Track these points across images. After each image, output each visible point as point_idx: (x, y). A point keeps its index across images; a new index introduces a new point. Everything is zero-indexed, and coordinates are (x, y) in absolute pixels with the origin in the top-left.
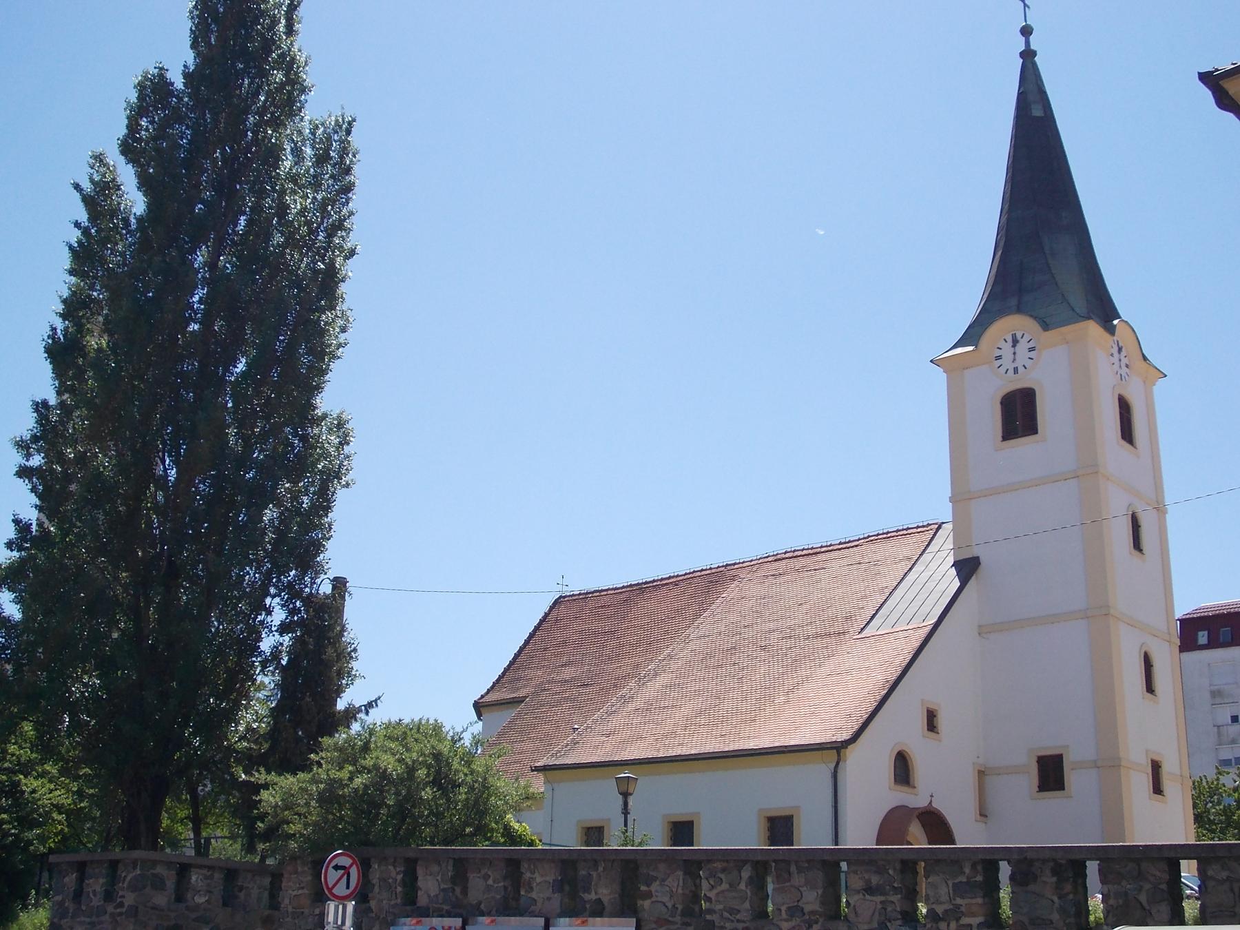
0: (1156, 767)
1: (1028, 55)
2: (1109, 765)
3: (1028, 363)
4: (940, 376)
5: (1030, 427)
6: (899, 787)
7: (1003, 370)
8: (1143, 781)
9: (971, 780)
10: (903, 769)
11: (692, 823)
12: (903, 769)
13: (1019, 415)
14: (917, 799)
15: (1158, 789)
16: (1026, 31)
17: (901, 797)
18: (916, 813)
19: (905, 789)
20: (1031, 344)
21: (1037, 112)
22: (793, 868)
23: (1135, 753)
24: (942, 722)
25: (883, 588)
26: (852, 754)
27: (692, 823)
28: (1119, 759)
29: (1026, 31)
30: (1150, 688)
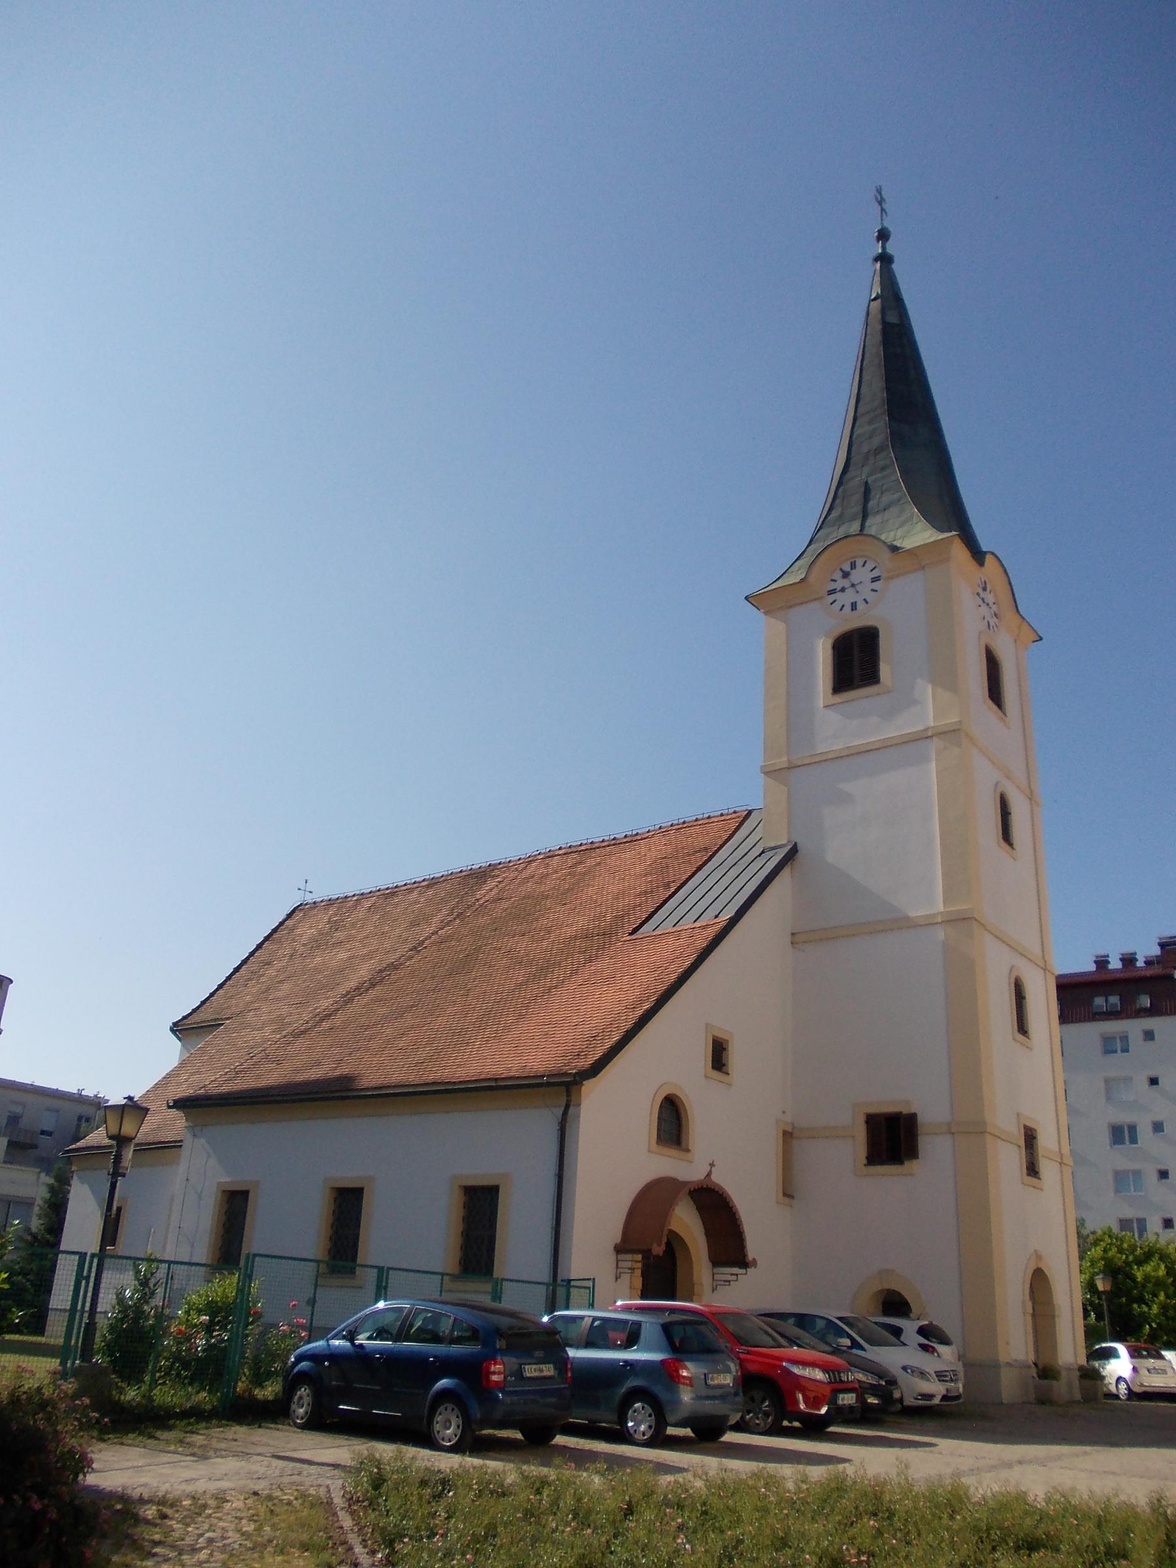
0: (1030, 1137)
1: (885, 259)
2: (972, 1130)
3: (870, 596)
4: (751, 1255)
5: (870, 676)
6: (666, 1150)
7: (837, 606)
8: (1009, 1159)
9: (771, 1146)
10: (672, 1121)
11: (362, 1189)
12: (672, 1121)
13: (856, 661)
14: (690, 1170)
15: (1032, 1170)
16: (883, 235)
17: (666, 1165)
18: (686, 1190)
19: (673, 1152)
20: (875, 574)
21: (893, 319)
22: (167, 1311)
23: (1003, 1120)
24: (735, 1058)
25: (669, 883)
26: (593, 1094)
27: (362, 1189)
28: (985, 1123)
29: (885, 259)
30: (1022, 1027)
